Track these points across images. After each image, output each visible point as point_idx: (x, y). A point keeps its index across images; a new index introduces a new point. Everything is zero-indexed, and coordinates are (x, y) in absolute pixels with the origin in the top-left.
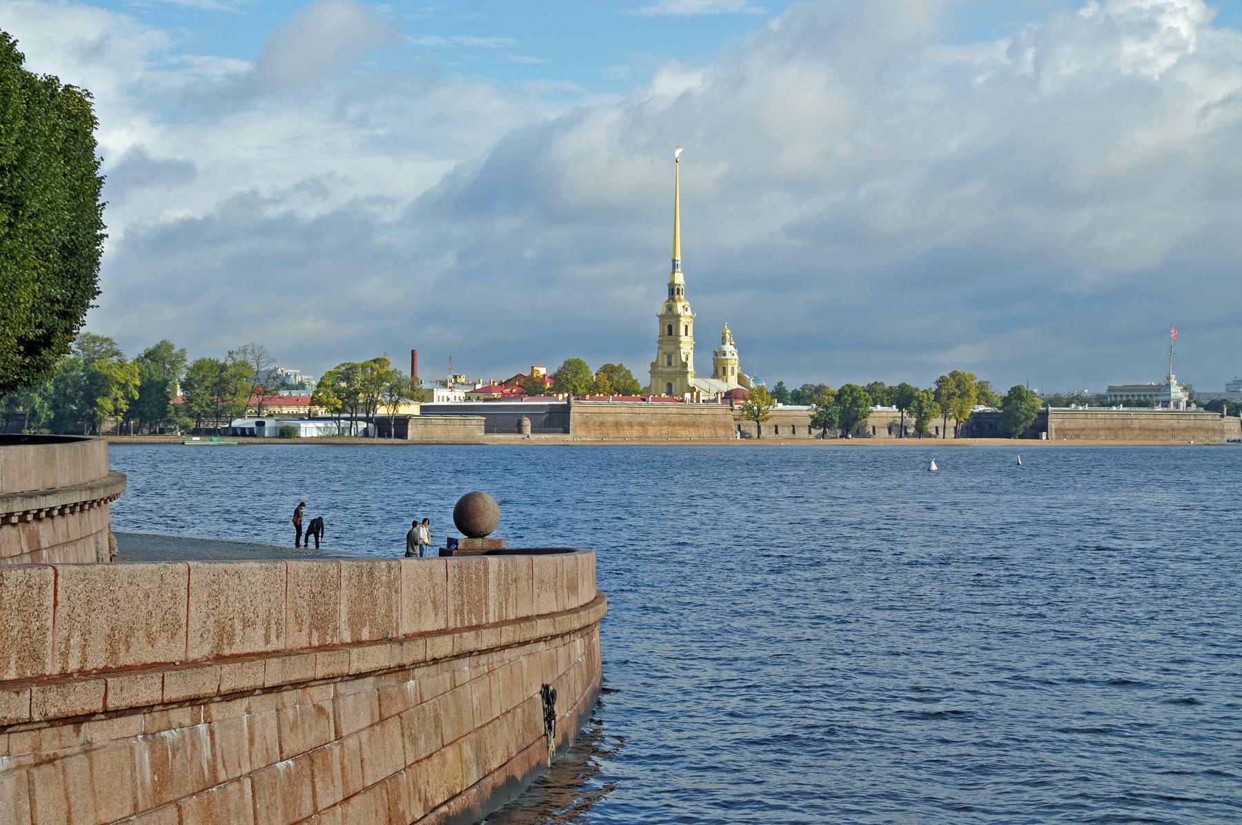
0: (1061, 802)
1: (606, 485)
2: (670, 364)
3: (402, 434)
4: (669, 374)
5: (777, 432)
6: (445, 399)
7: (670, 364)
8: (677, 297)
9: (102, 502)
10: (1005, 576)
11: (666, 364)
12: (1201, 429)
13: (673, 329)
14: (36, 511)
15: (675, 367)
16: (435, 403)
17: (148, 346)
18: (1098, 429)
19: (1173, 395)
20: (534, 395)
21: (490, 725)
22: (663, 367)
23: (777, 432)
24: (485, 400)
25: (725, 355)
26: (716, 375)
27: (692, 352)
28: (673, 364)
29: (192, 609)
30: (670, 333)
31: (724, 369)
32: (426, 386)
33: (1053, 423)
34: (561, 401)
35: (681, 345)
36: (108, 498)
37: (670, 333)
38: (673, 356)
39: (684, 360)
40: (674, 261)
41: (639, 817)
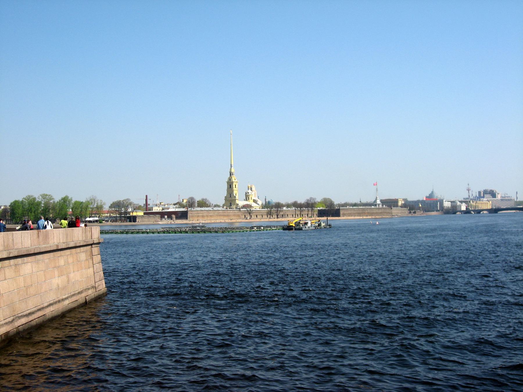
0: (269, 326)
1: (282, 243)
2: (231, 197)
3: (135, 221)
5: (257, 217)
7: (231, 197)
8: (232, 176)
12: (385, 212)
16: (154, 211)
17: (298, 201)
18: (355, 214)
19: (378, 203)
23: (257, 217)
25: (249, 193)
26: (246, 200)
27: (237, 193)
30: (230, 187)
31: (249, 198)
32: (151, 206)
33: (341, 212)
35: (234, 191)
37: (230, 187)
39: (235, 195)
40: (231, 165)
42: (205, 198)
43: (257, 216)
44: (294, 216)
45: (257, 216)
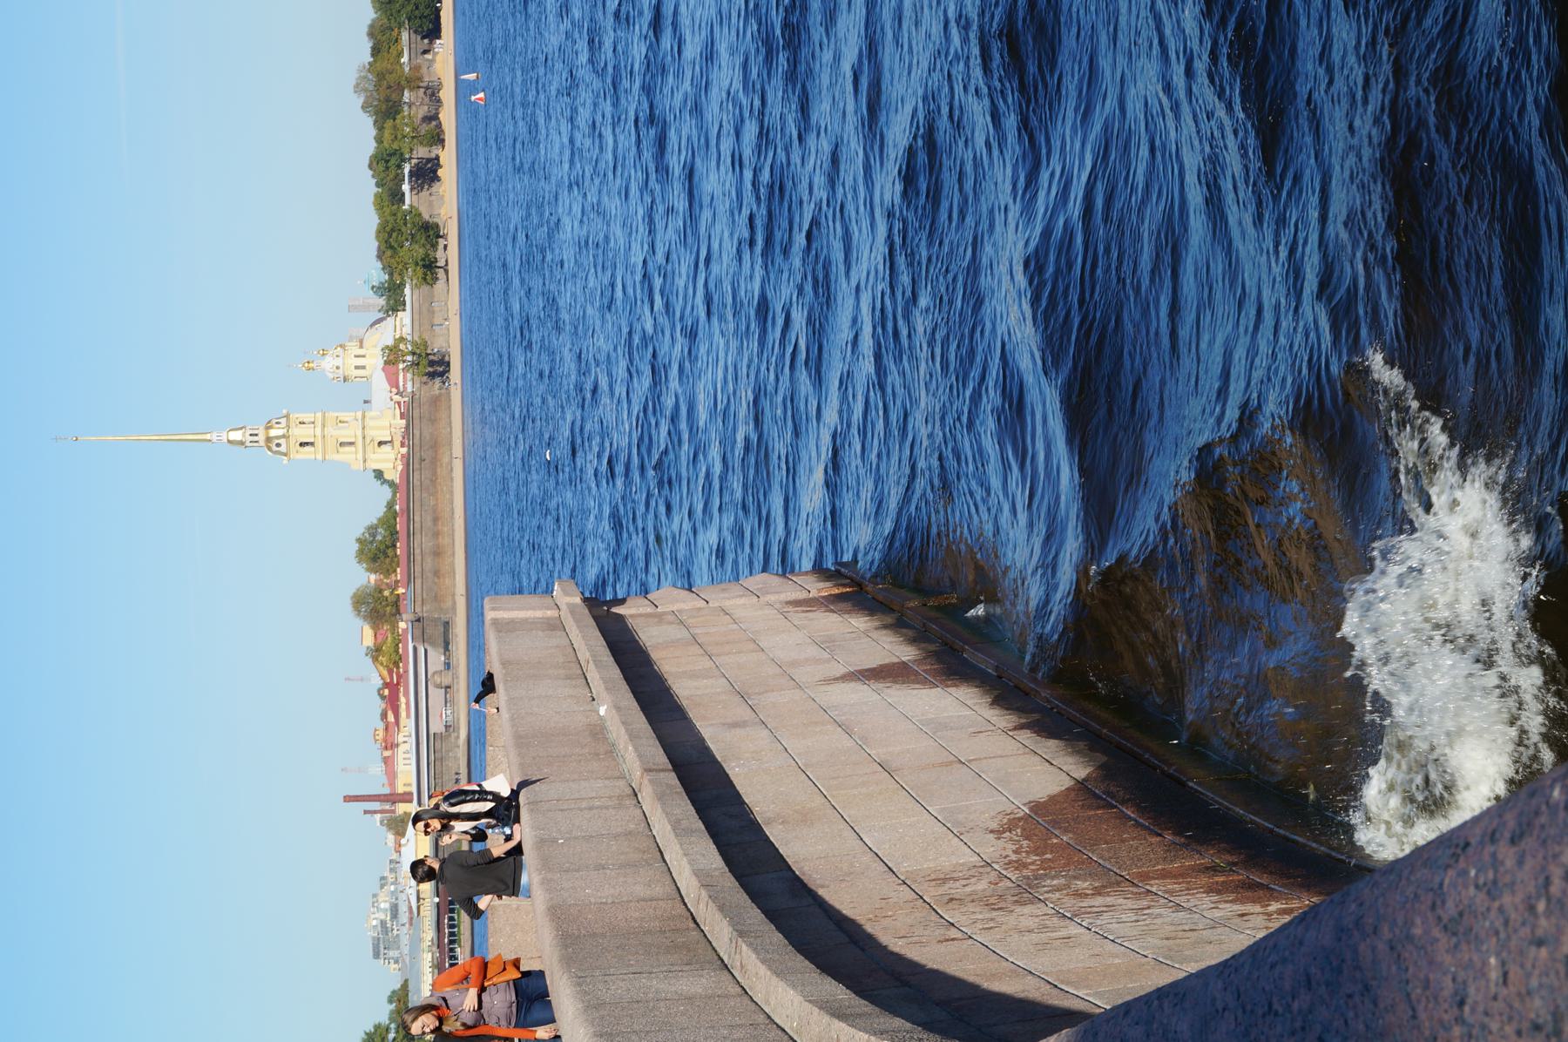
2: (351, 444)
7: (351, 444)
38: (341, 440)
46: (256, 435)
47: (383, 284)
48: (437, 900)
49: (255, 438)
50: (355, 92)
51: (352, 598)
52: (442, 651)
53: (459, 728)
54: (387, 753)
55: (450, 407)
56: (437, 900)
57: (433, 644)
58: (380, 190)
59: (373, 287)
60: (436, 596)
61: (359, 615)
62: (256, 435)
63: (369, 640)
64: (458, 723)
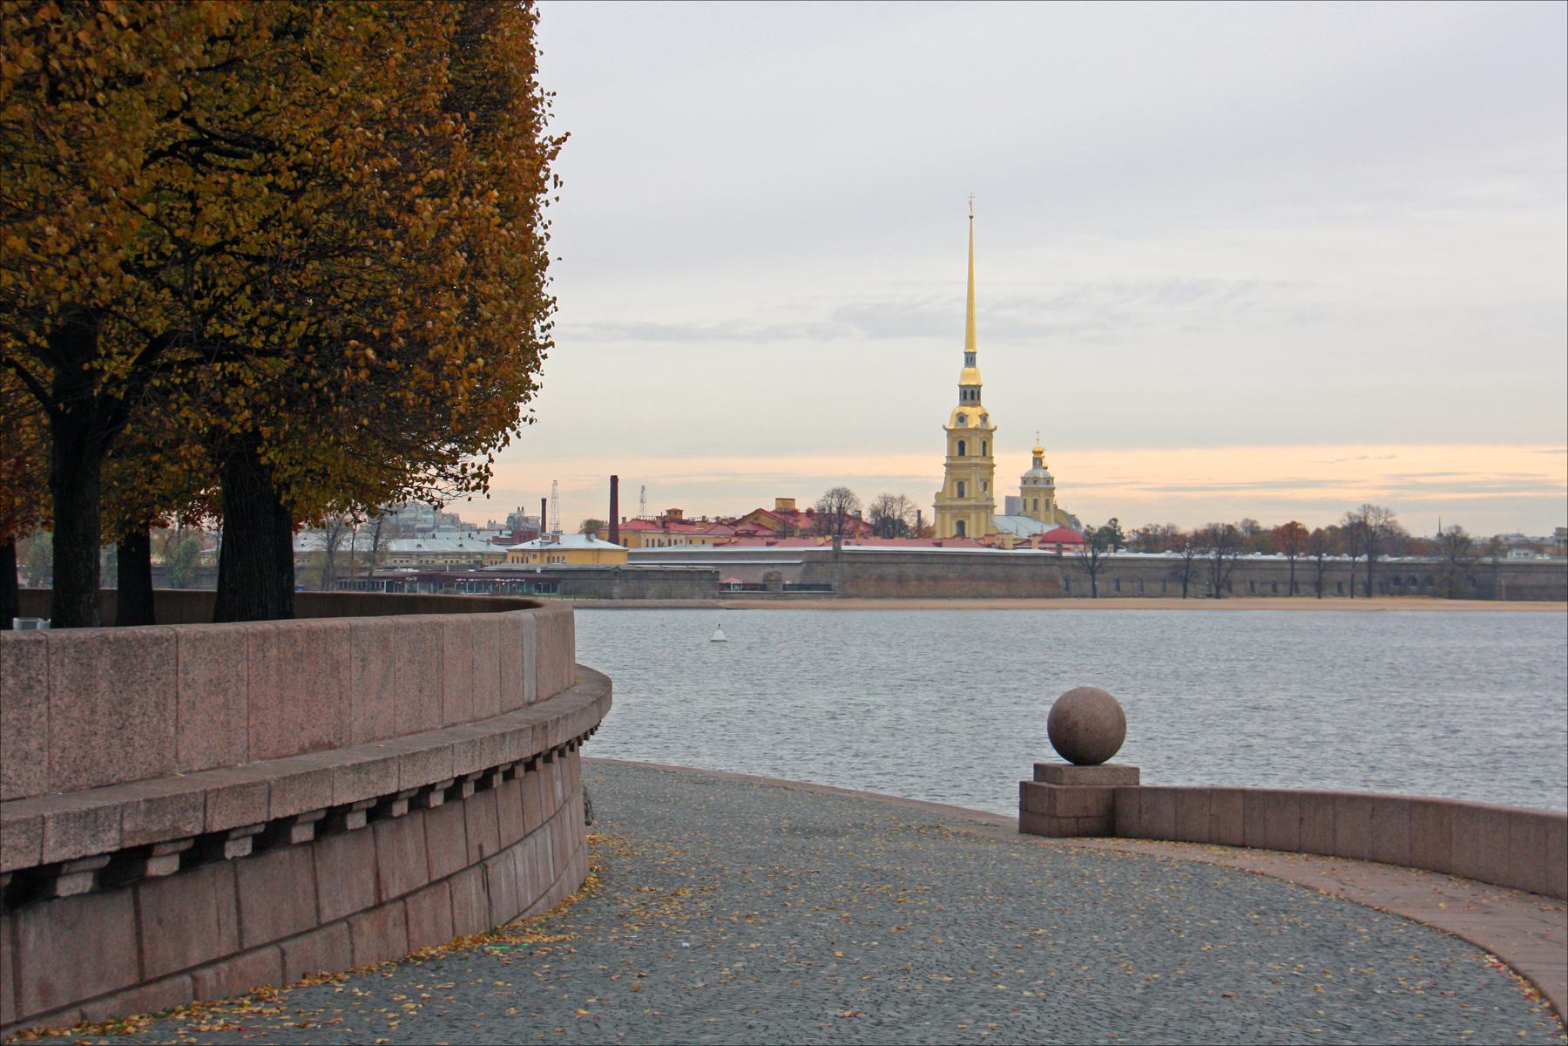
2: (961, 494)
4: (961, 508)
6: (656, 544)
7: (961, 494)
9: (556, 754)
10: (967, 720)
11: (956, 495)
13: (956, 452)
14: (451, 783)
15: (969, 499)
20: (892, 538)
21: (224, 966)
22: (951, 499)
24: (716, 545)
28: (966, 495)
29: (456, 911)
34: (977, 542)
36: (568, 743)
38: (966, 484)
41: (969, 1043)
42: (897, 495)
43: (1118, 581)
44: (1346, 588)
45: (1118, 581)
46: (653, 541)
47: (1119, 530)
48: (539, 571)
49: (650, 544)
50: (1364, 506)
51: (844, 489)
52: (797, 582)
53: (723, 598)
54: (798, 533)
55: (1047, 596)
56: (539, 571)
57: (805, 572)
58: (1082, 531)
59: (1115, 520)
60: (857, 577)
61: (828, 495)
62: (653, 541)
63: (801, 507)
64: (728, 598)
